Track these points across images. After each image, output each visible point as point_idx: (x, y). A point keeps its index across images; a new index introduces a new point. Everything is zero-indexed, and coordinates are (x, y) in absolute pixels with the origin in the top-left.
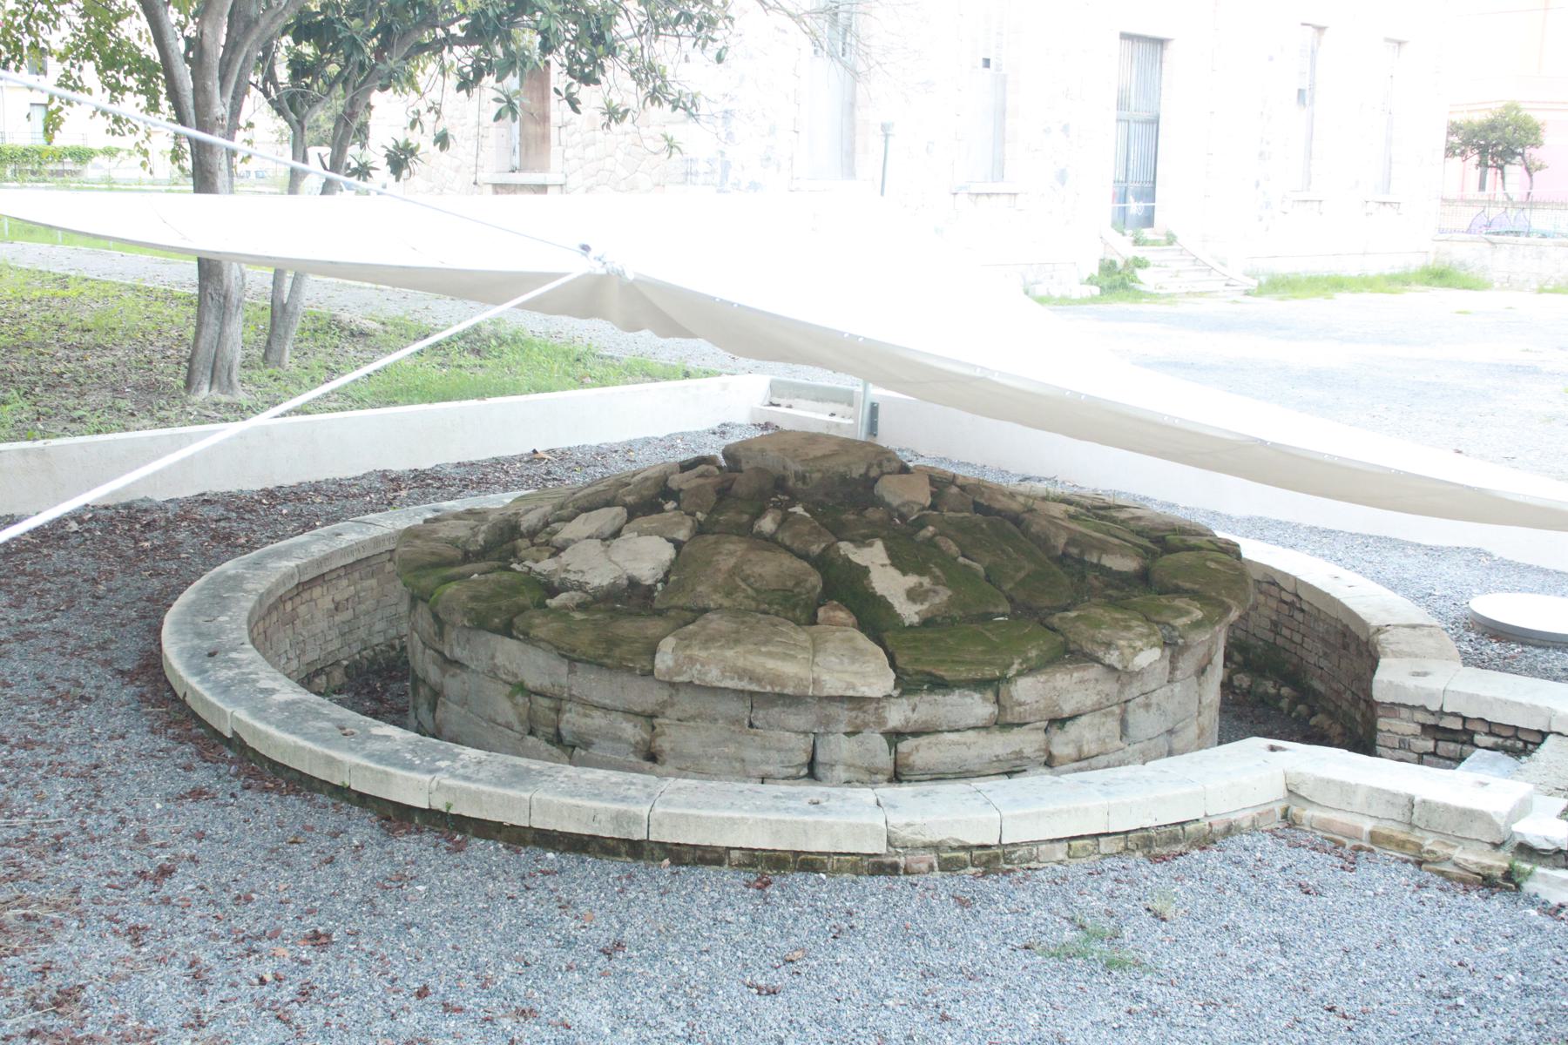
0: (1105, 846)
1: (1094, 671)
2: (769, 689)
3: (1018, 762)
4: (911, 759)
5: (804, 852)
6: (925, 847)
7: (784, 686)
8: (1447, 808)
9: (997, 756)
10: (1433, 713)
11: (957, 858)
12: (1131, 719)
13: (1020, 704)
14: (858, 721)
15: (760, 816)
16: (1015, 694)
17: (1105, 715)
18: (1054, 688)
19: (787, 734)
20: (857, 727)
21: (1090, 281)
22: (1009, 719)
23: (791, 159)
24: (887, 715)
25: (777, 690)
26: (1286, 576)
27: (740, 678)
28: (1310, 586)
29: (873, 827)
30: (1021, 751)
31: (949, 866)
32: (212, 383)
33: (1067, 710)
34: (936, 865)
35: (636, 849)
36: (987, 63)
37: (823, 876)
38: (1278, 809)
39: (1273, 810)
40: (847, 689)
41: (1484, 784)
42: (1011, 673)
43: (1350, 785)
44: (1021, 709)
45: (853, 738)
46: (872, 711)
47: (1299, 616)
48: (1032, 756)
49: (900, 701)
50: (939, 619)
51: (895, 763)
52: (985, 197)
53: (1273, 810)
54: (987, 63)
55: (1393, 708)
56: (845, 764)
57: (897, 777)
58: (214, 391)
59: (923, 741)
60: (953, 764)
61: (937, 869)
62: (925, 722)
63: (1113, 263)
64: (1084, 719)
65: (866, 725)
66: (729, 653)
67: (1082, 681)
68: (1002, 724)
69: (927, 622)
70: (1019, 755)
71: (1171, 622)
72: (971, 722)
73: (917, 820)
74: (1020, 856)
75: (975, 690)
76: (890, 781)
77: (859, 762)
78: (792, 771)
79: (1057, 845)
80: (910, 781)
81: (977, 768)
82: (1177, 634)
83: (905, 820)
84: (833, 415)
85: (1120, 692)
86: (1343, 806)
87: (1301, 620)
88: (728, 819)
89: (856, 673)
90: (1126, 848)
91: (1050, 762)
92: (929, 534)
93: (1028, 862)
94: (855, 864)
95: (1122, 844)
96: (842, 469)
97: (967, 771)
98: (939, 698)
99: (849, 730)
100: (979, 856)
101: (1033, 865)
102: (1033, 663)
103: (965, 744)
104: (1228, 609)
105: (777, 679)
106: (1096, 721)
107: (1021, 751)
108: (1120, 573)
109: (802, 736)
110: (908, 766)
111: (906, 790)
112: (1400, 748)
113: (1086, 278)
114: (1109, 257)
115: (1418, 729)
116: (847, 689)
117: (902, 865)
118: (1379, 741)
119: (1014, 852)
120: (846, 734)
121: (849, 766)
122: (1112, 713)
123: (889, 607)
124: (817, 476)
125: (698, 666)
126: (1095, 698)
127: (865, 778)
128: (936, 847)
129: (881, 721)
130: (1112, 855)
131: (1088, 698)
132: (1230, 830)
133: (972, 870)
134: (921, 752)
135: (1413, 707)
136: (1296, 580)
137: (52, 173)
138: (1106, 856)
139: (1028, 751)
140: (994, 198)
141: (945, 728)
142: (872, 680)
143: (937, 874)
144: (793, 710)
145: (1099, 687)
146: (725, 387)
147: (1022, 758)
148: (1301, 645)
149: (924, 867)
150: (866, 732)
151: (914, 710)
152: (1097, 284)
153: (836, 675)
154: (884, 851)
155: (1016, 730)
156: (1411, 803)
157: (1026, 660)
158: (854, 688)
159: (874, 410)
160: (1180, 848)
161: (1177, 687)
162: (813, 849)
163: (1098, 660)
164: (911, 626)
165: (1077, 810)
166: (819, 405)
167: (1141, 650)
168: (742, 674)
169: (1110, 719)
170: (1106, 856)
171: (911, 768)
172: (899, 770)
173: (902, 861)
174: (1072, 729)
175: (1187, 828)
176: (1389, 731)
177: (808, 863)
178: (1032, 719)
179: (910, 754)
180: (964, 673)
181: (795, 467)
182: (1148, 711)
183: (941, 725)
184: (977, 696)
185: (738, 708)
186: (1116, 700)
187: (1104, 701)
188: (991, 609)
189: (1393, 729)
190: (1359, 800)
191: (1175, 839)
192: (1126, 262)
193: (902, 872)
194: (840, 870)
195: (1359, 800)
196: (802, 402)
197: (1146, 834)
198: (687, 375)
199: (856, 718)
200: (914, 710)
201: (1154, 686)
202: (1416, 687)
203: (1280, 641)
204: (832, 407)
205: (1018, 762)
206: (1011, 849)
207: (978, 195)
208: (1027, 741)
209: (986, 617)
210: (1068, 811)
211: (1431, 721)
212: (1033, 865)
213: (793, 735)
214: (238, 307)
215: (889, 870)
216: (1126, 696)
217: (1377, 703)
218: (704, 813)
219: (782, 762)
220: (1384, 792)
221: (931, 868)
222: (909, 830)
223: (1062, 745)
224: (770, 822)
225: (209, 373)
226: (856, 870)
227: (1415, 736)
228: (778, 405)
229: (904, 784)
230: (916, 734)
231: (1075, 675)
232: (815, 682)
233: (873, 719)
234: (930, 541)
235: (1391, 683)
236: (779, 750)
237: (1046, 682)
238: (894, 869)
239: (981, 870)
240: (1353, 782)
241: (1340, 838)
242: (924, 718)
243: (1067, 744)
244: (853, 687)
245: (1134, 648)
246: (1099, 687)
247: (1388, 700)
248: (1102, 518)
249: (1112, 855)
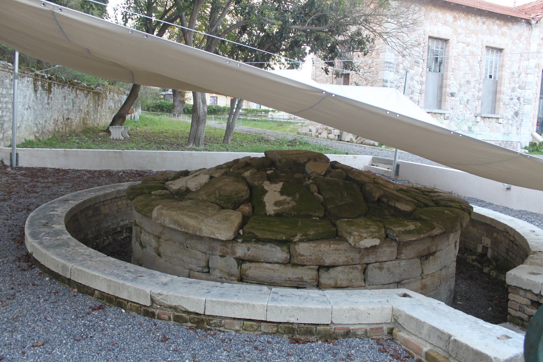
0: (263, 326)
1: (343, 246)
2: (183, 230)
3: (301, 283)
4: (247, 272)
5: (120, 298)
6: (170, 307)
7: (189, 229)
8: (467, 347)
9: (289, 278)
10: (537, 295)
11: (182, 316)
12: (369, 272)
13: (303, 255)
14: (224, 251)
15: (104, 276)
16: (298, 250)
17: (353, 268)
18: (320, 250)
19: (198, 252)
20: (224, 254)
21: (526, 148)
22: (295, 261)
23: (418, 102)
24: (236, 250)
25: (186, 231)
26: (511, 228)
27: (175, 224)
28: (519, 233)
29: (144, 292)
30: (302, 278)
31: (178, 319)
32: (194, 143)
33: (328, 261)
34: (172, 317)
35: (70, 282)
36: (491, 77)
37: (123, 311)
38: (385, 328)
39: (382, 328)
40: (211, 234)
41: (508, 337)
42: (296, 239)
43: (421, 322)
44: (302, 258)
45: (223, 259)
46: (230, 247)
47: (515, 247)
48: (309, 281)
49: (242, 244)
50: (285, 214)
51: (240, 273)
52: (487, 119)
53: (382, 328)
54: (491, 77)
55: (517, 289)
56: (219, 269)
57: (242, 279)
58: (194, 145)
59: (253, 265)
60: (267, 278)
61: (172, 320)
62: (253, 256)
63: (535, 144)
64: (202, 251)
65: (227, 253)
66: (174, 213)
67: (336, 250)
68: (290, 263)
69: (278, 215)
70: (301, 280)
71: (393, 229)
72: (276, 260)
73: (165, 293)
74: (215, 323)
75: (278, 245)
76: (238, 281)
77: (224, 270)
78: (200, 269)
79: (236, 322)
80: (247, 282)
81: (279, 282)
82: (395, 235)
83: (159, 291)
84: (388, 169)
85: (360, 258)
86: (417, 334)
87: (516, 249)
88: (94, 275)
89: (216, 228)
90: (277, 331)
91: (319, 286)
92: (309, 183)
93: (220, 327)
94: (137, 308)
95: (275, 329)
96: (294, 159)
97: (274, 283)
98: (260, 246)
99: (221, 254)
100: (193, 318)
101: (221, 329)
102: (311, 237)
103: (273, 270)
104: (433, 228)
105: (186, 226)
106: (347, 270)
107: (302, 278)
108: (404, 211)
109: (203, 254)
110: (245, 275)
111: (244, 286)
112: (519, 311)
113: (524, 147)
114: (534, 142)
115: (529, 303)
116: (211, 234)
117: (156, 314)
118: (509, 305)
119: (212, 320)
120: (220, 256)
121: (221, 271)
122: (357, 268)
123: (265, 206)
124: (284, 160)
125: (163, 217)
126: (345, 259)
127: (227, 277)
128: (175, 308)
129: (234, 253)
130: (267, 334)
131: (342, 259)
132: (348, 334)
133: (189, 324)
134: (252, 270)
135: (525, 290)
136: (514, 231)
137: (258, 116)
138: (264, 333)
139: (305, 278)
140: (490, 119)
141: (262, 260)
142: (222, 232)
143: (172, 322)
144: (199, 242)
145: (347, 254)
146: (355, 158)
147: (303, 281)
148: (515, 260)
149: (166, 317)
150: (228, 257)
151: (248, 250)
152: (528, 149)
153: (208, 227)
154: (149, 304)
155: (300, 267)
156: (450, 336)
157: (306, 235)
158: (214, 234)
159: (398, 166)
160: (313, 338)
161: (403, 263)
162: (122, 297)
163: (347, 241)
164: (270, 216)
165: (248, 305)
166: (385, 166)
167: (366, 238)
168: (176, 222)
169: (356, 271)
170: (264, 333)
171: (247, 277)
172: (242, 277)
173: (157, 312)
174: (333, 273)
175: (318, 328)
176: (514, 301)
177: (119, 303)
178: (308, 263)
179: (246, 270)
180: (268, 235)
181: (279, 157)
182: (381, 271)
183: (260, 259)
184: (278, 248)
185: (181, 238)
186: (358, 262)
187: (350, 261)
188: (312, 213)
189: (516, 300)
190: (425, 331)
191: (311, 333)
192: (540, 143)
193: (156, 317)
194: (131, 310)
195: (425, 331)
196: (381, 165)
197: (291, 326)
198: (347, 154)
199: (224, 249)
200: (248, 250)
201: (385, 259)
202: (527, 279)
203: (508, 258)
204: (388, 166)
205: (301, 283)
206: (211, 318)
207: (485, 117)
208: (308, 274)
209: (310, 216)
210: (243, 305)
211: (535, 299)
212: (221, 329)
213: (200, 253)
214: (202, 121)
215: (150, 315)
216: (366, 260)
217: (509, 286)
218: (87, 270)
219: (196, 264)
220: (438, 330)
221: (170, 319)
222: (160, 297)
223: (325, 278)
224: (107, 280)
225: (193, 140)
226: (138, 311)
227: (527, 306)
228: (374, 165)
229: (245, 283)
230: (251, 261)
231: (332, 246)
232: (200, 229)
233: (230, 251)
234: (308, 187)
235: (515, 275)
236: (196, 259)
237: (316, 247)
238: (152, 315)
239: (194, 325)
240: (423, 320)
241: (412, 352)
242: (253, 254)
243: (329, 279)
244: (213, 233)
245: (361, 237)
246: (347, 254)
247: (513, 284)
248: (425, 195)
249: (267, 334)
